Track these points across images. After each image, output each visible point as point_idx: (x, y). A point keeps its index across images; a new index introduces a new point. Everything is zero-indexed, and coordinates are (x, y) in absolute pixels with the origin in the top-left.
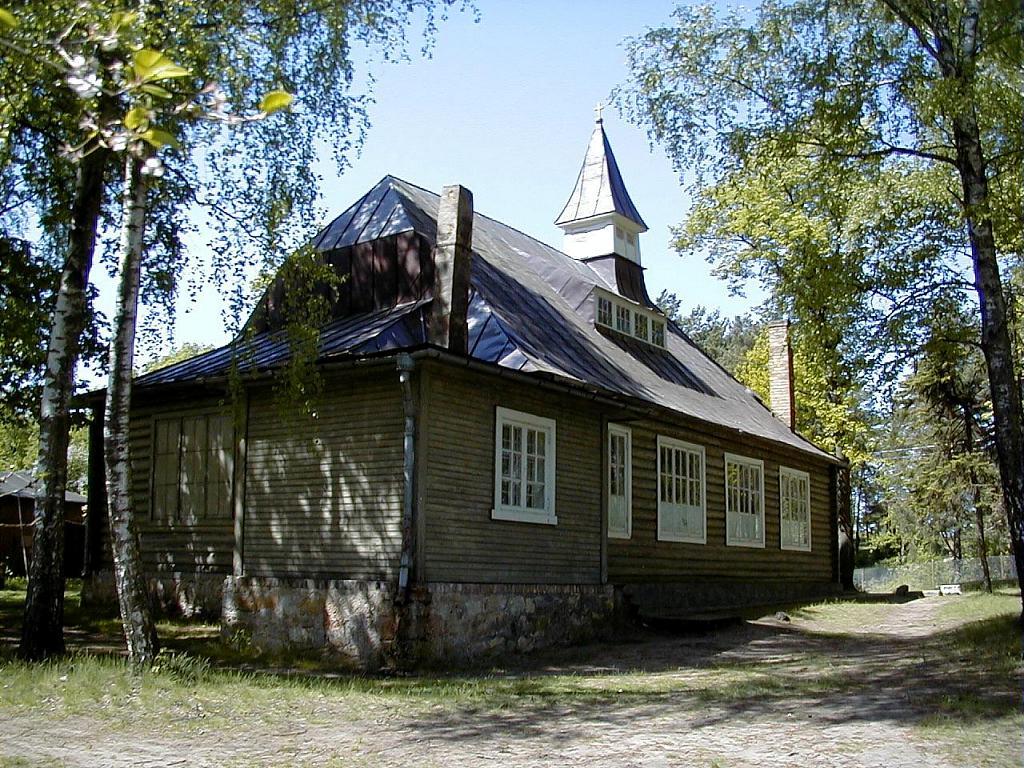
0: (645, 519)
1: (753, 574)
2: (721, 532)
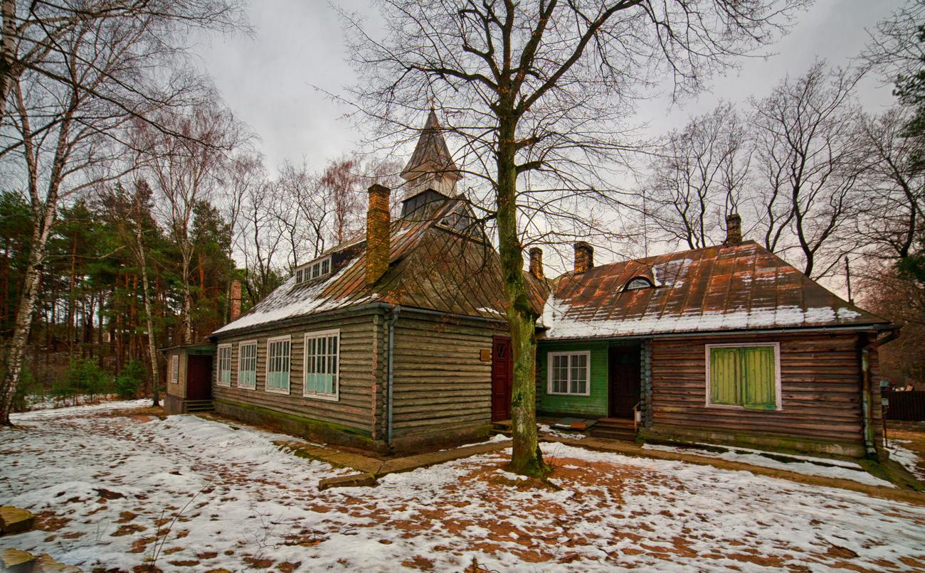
1: (285, 411)
2: (258, 379)
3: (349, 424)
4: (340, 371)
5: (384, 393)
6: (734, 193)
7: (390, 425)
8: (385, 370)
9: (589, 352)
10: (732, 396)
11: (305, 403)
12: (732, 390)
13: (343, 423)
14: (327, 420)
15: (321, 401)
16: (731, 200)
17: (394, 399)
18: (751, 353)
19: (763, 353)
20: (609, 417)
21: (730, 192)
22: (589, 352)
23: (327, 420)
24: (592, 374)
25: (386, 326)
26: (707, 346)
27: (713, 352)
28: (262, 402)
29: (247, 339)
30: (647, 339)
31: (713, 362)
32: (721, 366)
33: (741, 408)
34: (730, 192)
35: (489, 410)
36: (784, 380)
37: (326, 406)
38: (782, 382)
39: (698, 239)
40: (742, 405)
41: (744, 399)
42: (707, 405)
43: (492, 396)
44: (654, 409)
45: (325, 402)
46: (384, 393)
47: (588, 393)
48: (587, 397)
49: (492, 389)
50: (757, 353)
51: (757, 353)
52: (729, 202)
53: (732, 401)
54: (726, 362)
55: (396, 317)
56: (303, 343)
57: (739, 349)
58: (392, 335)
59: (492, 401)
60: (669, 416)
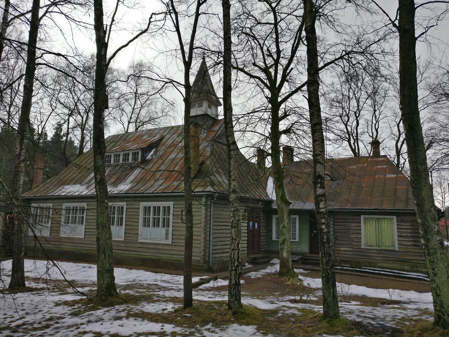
0: (55, 229)
3: (177, 256)
4: (126, 225)
5: (208, 238)
6: (377, 113)
7: (211, 256)
8: (209, 226)
9: (298, 216)
10: (375, 242)
11: (139, 245)
12: (375, 239)
13: (174, 256)
14: (160, 255)
15: (155, 244)
16: (376, 117)
17: (213, 242)
18: (383, 221)
19: (389, 221)
20: (310, 254)
21: (374, 113)
22: (298, 216)
23: (160, 255)
24: (300, 229)
25: (209, 203)
26: (362, 216)
27: (365, 219)
28: (91, 246)
29: (74, 202)
30: (332, 211)
31: (365, 222)
32: (369, 227)
33: (378, 248)
34: (374, 113)
35: (246, 249)
36: (399, 235)
37: (160, 247)
38: (398, 236)
39: (355, 140)
40: (379, 247)
41: (380, 244)
42: (363, 247)
43: (247, 240)
44: (335, 248)
45: (159, 244)
46: (208, 238)
47: (297, 240)
48: (297, 242)
49: (247, 237)
50: (386, 221)
51: (386, 221)
52: (374, 118)
53: (375, 245)
54: (371, 224)
55: (215, 199)
56: (139, 208)
57: (378, 219)
58: (212, 207)
59: (247, 244)
60: (343, 252)
